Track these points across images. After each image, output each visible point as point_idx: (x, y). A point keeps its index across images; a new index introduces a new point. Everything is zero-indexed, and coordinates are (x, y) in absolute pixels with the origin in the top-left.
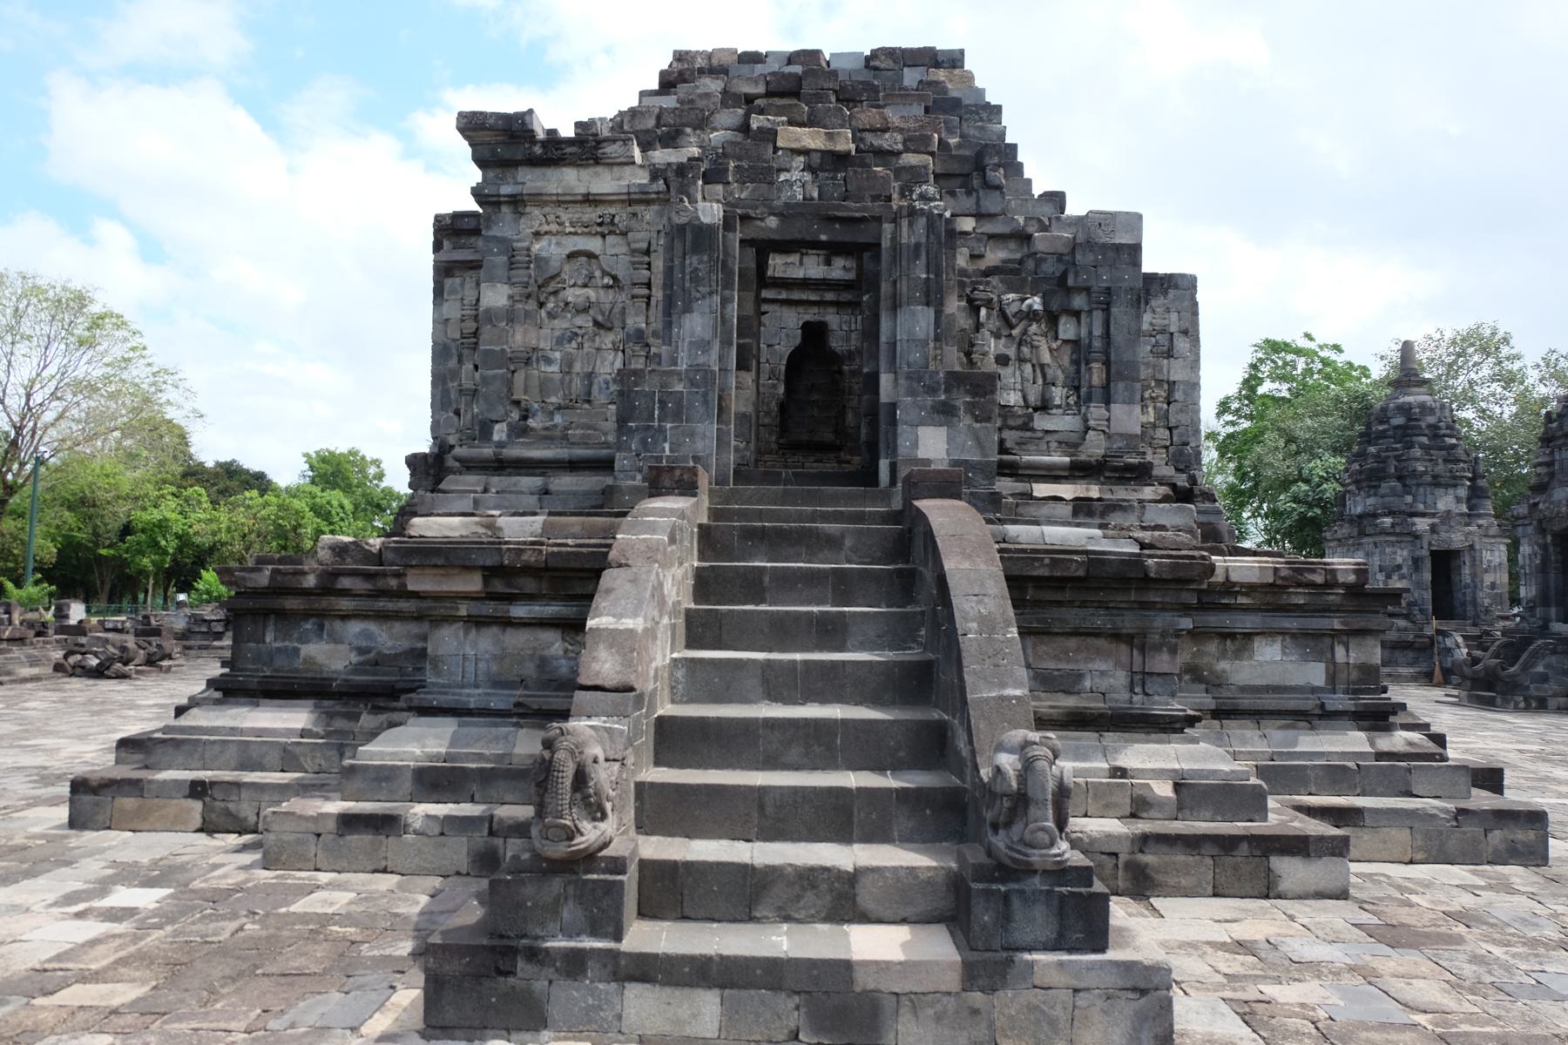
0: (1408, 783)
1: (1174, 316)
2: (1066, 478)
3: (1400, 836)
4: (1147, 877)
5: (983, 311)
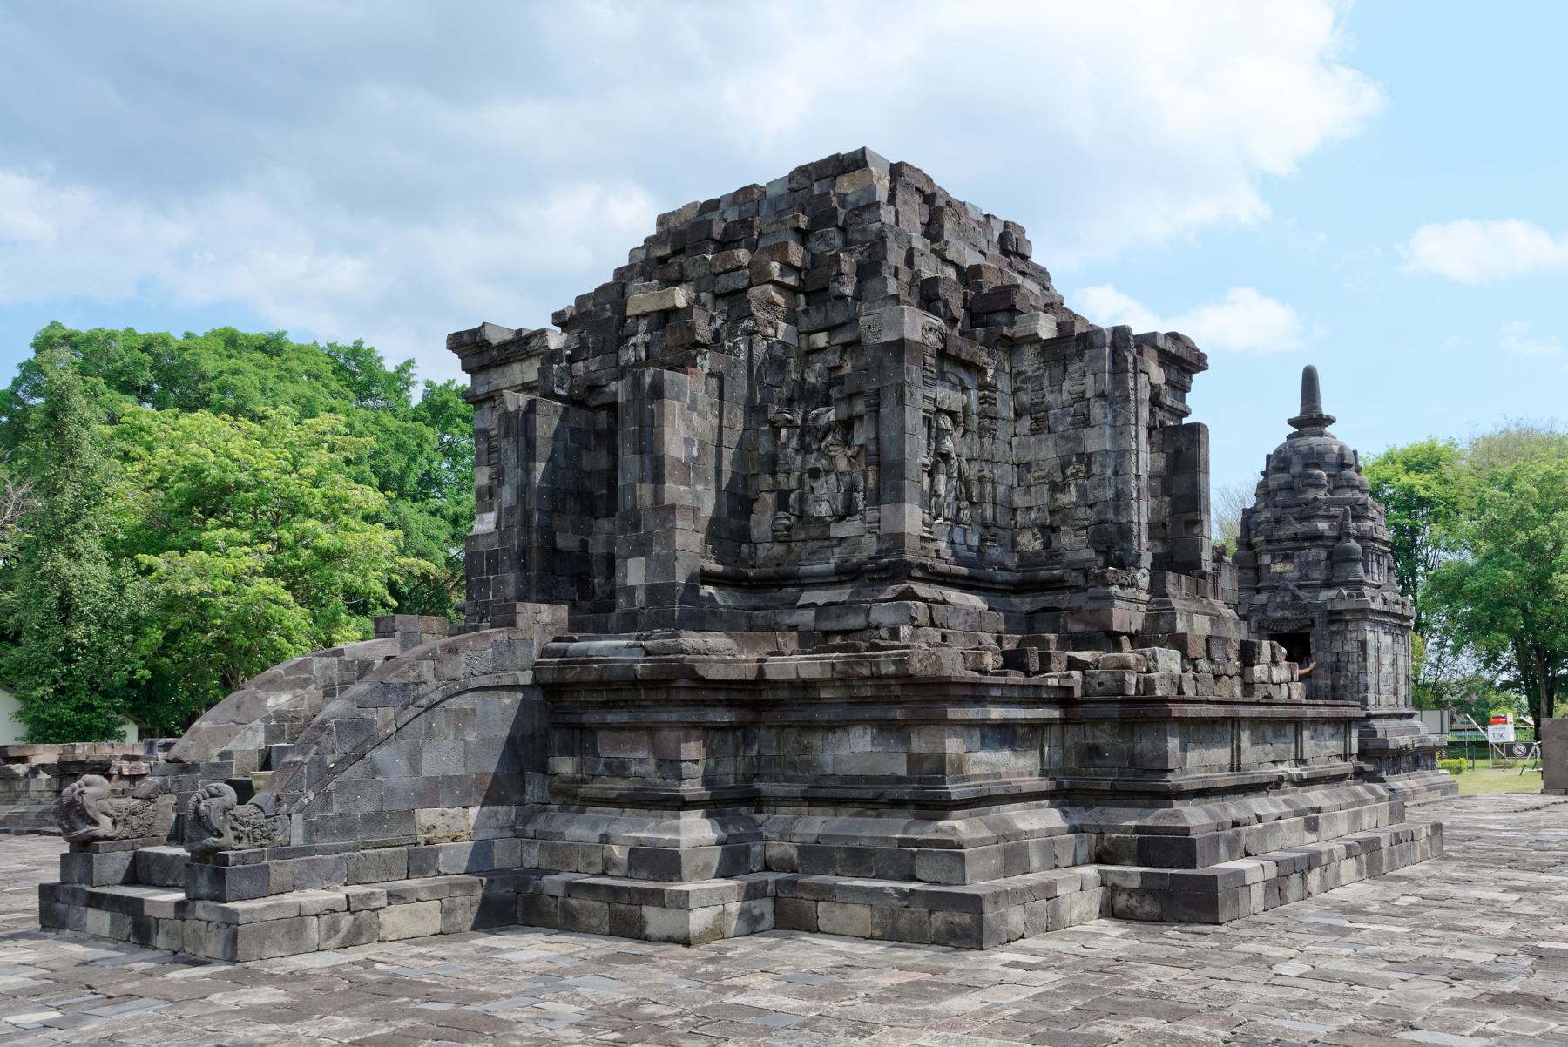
0: (912, 868)
1: (1090, 380)
2: (832, 583)
3: (861, 914)
4: (574, 918)
5: (784, 432)
